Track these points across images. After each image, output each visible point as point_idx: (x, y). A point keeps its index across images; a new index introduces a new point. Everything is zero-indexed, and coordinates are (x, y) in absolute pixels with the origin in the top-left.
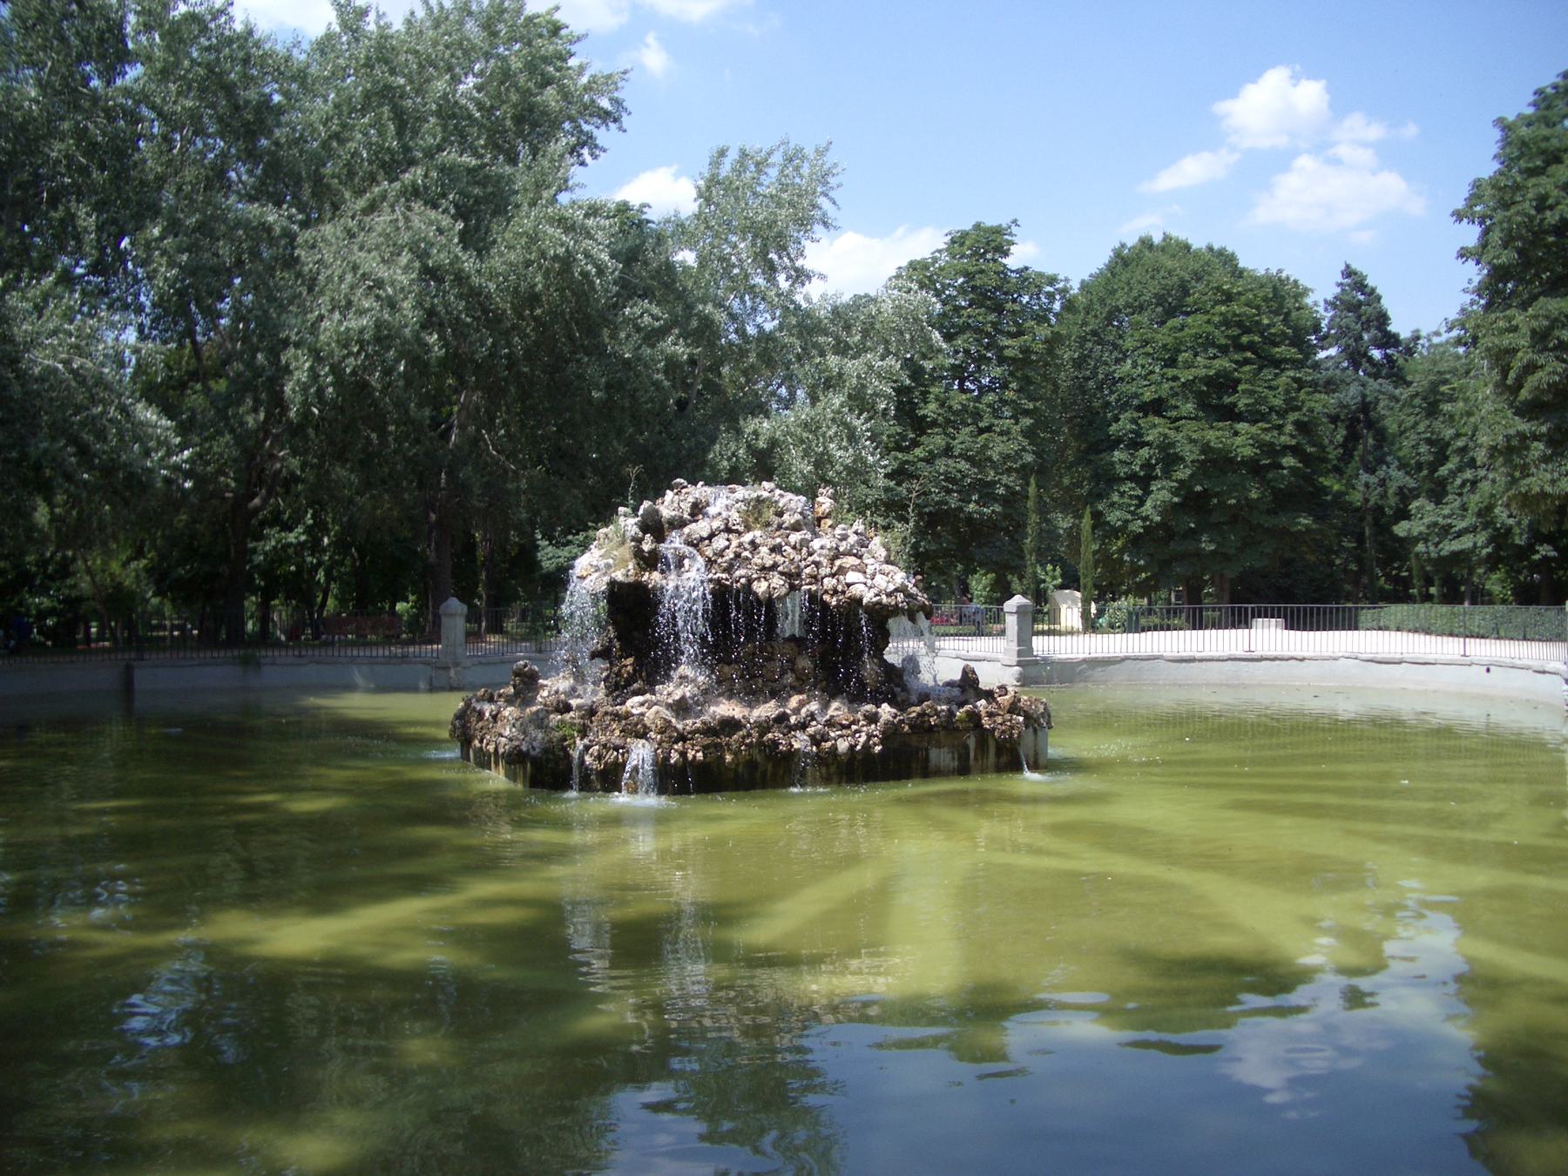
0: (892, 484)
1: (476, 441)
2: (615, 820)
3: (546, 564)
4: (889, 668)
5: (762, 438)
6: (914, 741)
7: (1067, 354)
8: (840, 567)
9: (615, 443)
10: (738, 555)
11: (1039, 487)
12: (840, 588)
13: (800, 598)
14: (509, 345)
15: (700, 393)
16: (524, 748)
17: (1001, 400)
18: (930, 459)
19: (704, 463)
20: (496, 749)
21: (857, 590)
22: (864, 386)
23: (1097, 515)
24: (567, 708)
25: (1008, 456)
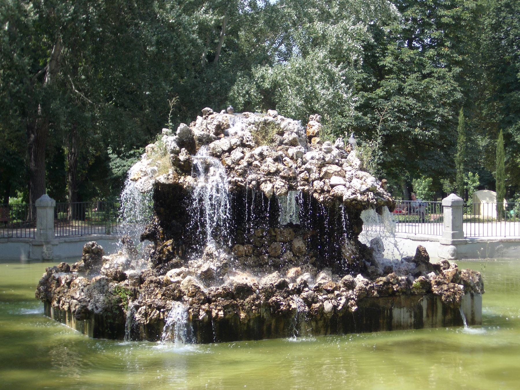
0: (360, 114)
1: (63, 84)
2: (156, 364)
3: (115, 171)
4: (362, 248)
5: (267, 81)
6: (381, 303)
7: (487, 21)
8: (326, 173)
9: (164, 84)
10: (250, 164)
11: (465, 116)
12: (326, 188)
13: (292, 196)
14: (86, 12)
15: (224, 50)
16: (90, 308)
17: (439, 55)
18: (387, 97)
19: (226, 99)
20: (69, 308)
21: (338, 190)
22: (341, 44)
23: (508, 137)
24: (123, 277)
25: (444, 94)
